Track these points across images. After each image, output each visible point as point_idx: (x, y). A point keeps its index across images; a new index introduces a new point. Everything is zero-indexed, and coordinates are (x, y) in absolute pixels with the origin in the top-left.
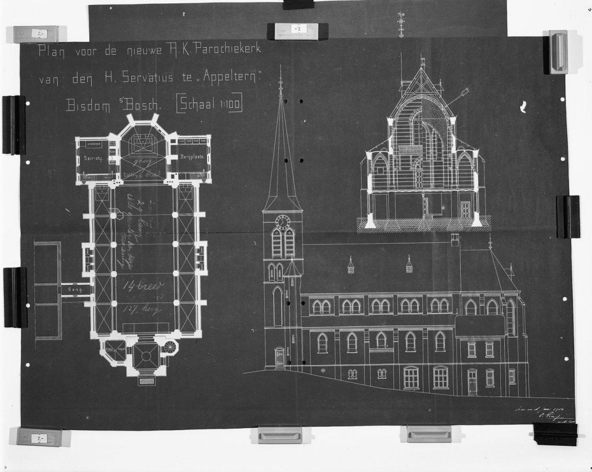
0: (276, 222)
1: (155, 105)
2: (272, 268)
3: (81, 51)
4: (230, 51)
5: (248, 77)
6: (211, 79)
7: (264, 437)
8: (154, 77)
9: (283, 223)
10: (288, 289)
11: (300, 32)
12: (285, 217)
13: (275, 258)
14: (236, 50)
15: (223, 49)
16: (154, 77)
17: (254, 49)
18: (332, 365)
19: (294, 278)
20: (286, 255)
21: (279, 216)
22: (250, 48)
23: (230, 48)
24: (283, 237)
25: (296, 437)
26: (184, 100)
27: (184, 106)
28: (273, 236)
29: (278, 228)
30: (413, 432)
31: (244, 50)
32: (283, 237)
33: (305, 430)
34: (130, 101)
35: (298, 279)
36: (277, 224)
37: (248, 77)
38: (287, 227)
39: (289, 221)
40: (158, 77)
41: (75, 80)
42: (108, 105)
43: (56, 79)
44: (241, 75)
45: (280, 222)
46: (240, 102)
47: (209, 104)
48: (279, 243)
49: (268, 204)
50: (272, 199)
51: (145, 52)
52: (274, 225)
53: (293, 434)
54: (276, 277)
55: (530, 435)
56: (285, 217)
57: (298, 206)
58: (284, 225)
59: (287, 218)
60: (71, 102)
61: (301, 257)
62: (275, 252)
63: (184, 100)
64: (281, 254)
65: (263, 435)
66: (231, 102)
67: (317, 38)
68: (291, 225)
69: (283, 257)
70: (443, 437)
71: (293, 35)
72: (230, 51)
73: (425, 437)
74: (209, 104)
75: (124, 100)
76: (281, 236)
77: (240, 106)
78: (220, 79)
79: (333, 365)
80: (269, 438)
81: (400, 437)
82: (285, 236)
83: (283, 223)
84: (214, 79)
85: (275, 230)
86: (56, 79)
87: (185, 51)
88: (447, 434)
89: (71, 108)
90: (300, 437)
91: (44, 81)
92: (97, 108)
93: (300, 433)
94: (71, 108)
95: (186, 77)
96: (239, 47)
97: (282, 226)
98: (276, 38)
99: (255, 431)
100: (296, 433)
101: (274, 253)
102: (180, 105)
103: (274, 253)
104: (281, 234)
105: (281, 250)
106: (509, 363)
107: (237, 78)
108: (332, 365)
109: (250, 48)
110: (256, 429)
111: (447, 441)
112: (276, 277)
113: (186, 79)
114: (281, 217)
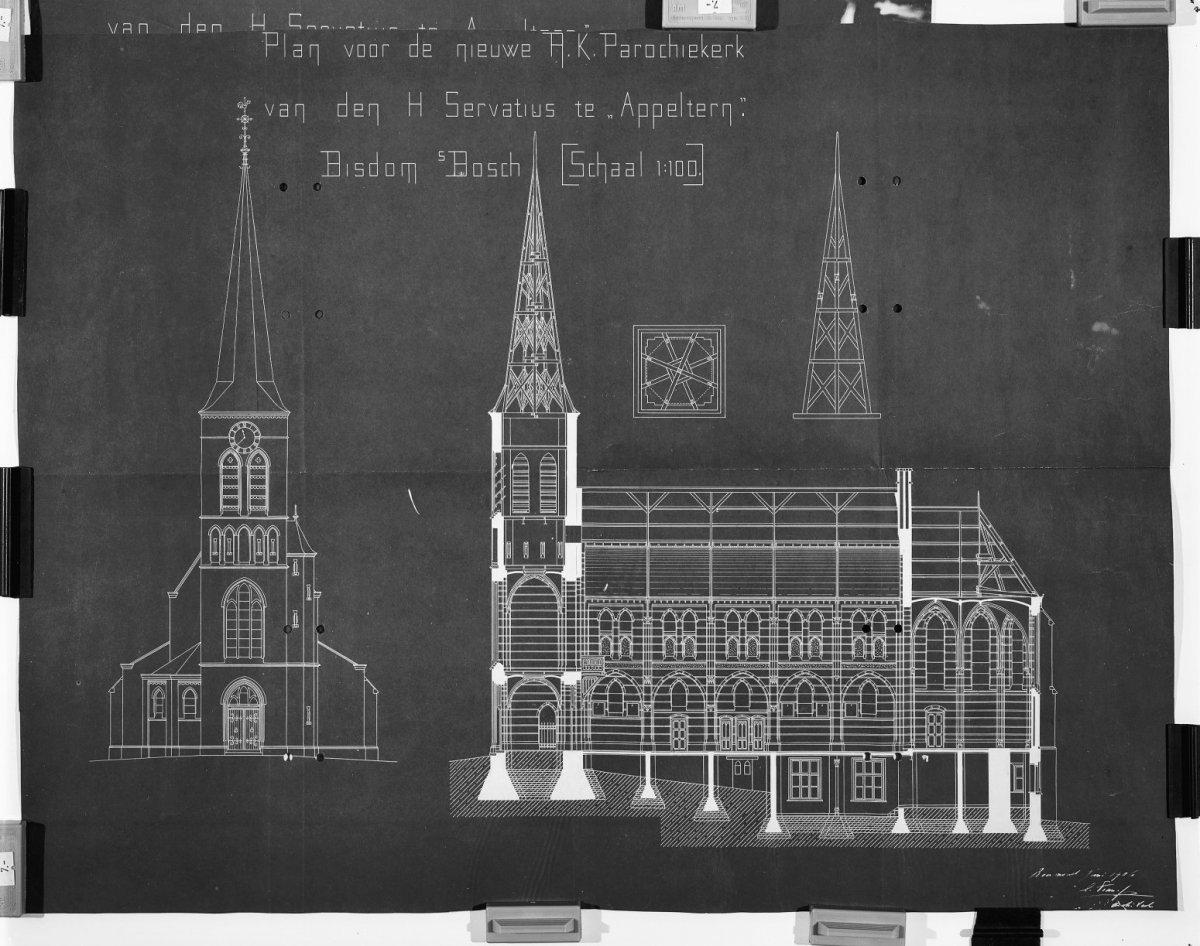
0: (229, 437)
1: (515, 167)
2: (216, 534)
3: (355, 48)
4: (680, 53)
5: (717, 110)
6: (636, 112)
7: (498, 929)
8: (514, 108)
9: (246, 440)
10: (311, 582)
11: (718, 11)
12: (248, 425)
13: (254, 514)
14: (691, 51)
15: (665, 50)
16: (514, 108)
17: (732, 51)
18: (160, 747)
19: (300, 560)
20: (250, 507)
21: (237, 424)
22: (723, 48)
23: (468, 48)
24: (244, 469)
25: (568, 927)
26: (578, 158)
27: (578, 170)
28: (222, 466)
29: (234, 450)
30: (824, 923)
31: (708, 51)
32: (244, 469)
33: (587, 916)
34: (460, 158)
35: (309, 560)
36: (232, 441)
37: (717, 110)
38: (253, 447)
39: (257, 434)
40: (521, 109)
41: (342, 109)
42: (479, 166)
43: (299, 108)
44: (701, 108)
45: (238, 436)
46: (699, 164)
47: (630, 167)
48: (235, 482)
49: (213, 399)
50: (220, 388)
51: (495, 53)
52: (226, 444)
53: (562, 922)
54: (222, 554)
55: (963, 933)
56: (248, 425)
57: (277, 401)
58: (248, 442)
59: (253, 428)
60: (333, 158)
61: (284, 514)
62: (226, 502)
63: (578, 158)
64: (239, 507)
65: (496, 925)
66: (679, 164)
67: (753, 25)
68: (264, 444)
69: (244, 512)
70: (887, 936)
71: (702, 17)
72: (680, 53)
73: (847, 934)
74: (630, 167)
75: (449, 157)
76: (239, 467)
77: (699, 170)
78: (657, 113)
79: (163, 747)
80: (512, 930)
81: (794, 932)
82: (249, 467)
83: (246, 440)
84: (643, 113)
85: (229, 453)
86: (299, 108)
87: (581, 51)
88: (897, 929)
89: (334, 169)
90: (576, 927)
91: (499, 112)
92: (390, 172)
93: (577, 918)
94: (334, 169)
95: (582, 109)
96: (699, 46)
97: (241, 445)
98: (666, 23)
99: (481, 917)
100: (569, 920)
101: (224, 504)
102: (569, 169)
103: (224, 504)
104: (239, 463)
105: (239, 497)
106: (165, 747)
107: (694, 112)
108: (160, 747)
109: (723, 48)
110: (482, 913)
111: (567, 939)
112: (222, 554)
113: (582, 113)
114: (241, 425)
